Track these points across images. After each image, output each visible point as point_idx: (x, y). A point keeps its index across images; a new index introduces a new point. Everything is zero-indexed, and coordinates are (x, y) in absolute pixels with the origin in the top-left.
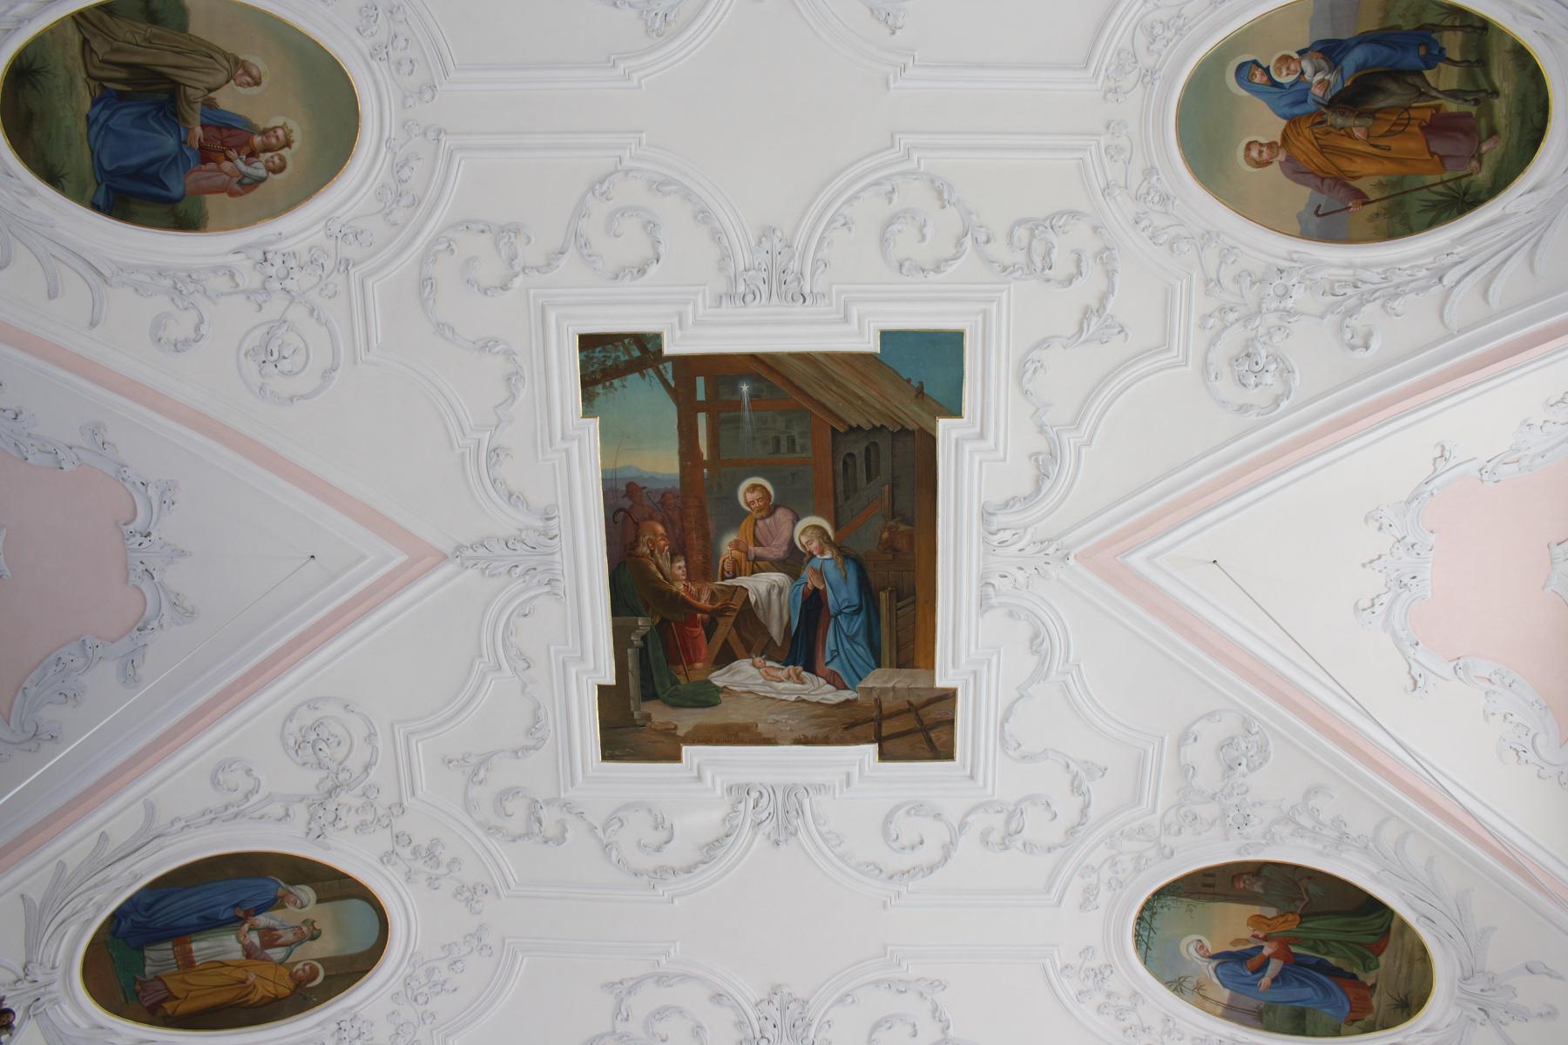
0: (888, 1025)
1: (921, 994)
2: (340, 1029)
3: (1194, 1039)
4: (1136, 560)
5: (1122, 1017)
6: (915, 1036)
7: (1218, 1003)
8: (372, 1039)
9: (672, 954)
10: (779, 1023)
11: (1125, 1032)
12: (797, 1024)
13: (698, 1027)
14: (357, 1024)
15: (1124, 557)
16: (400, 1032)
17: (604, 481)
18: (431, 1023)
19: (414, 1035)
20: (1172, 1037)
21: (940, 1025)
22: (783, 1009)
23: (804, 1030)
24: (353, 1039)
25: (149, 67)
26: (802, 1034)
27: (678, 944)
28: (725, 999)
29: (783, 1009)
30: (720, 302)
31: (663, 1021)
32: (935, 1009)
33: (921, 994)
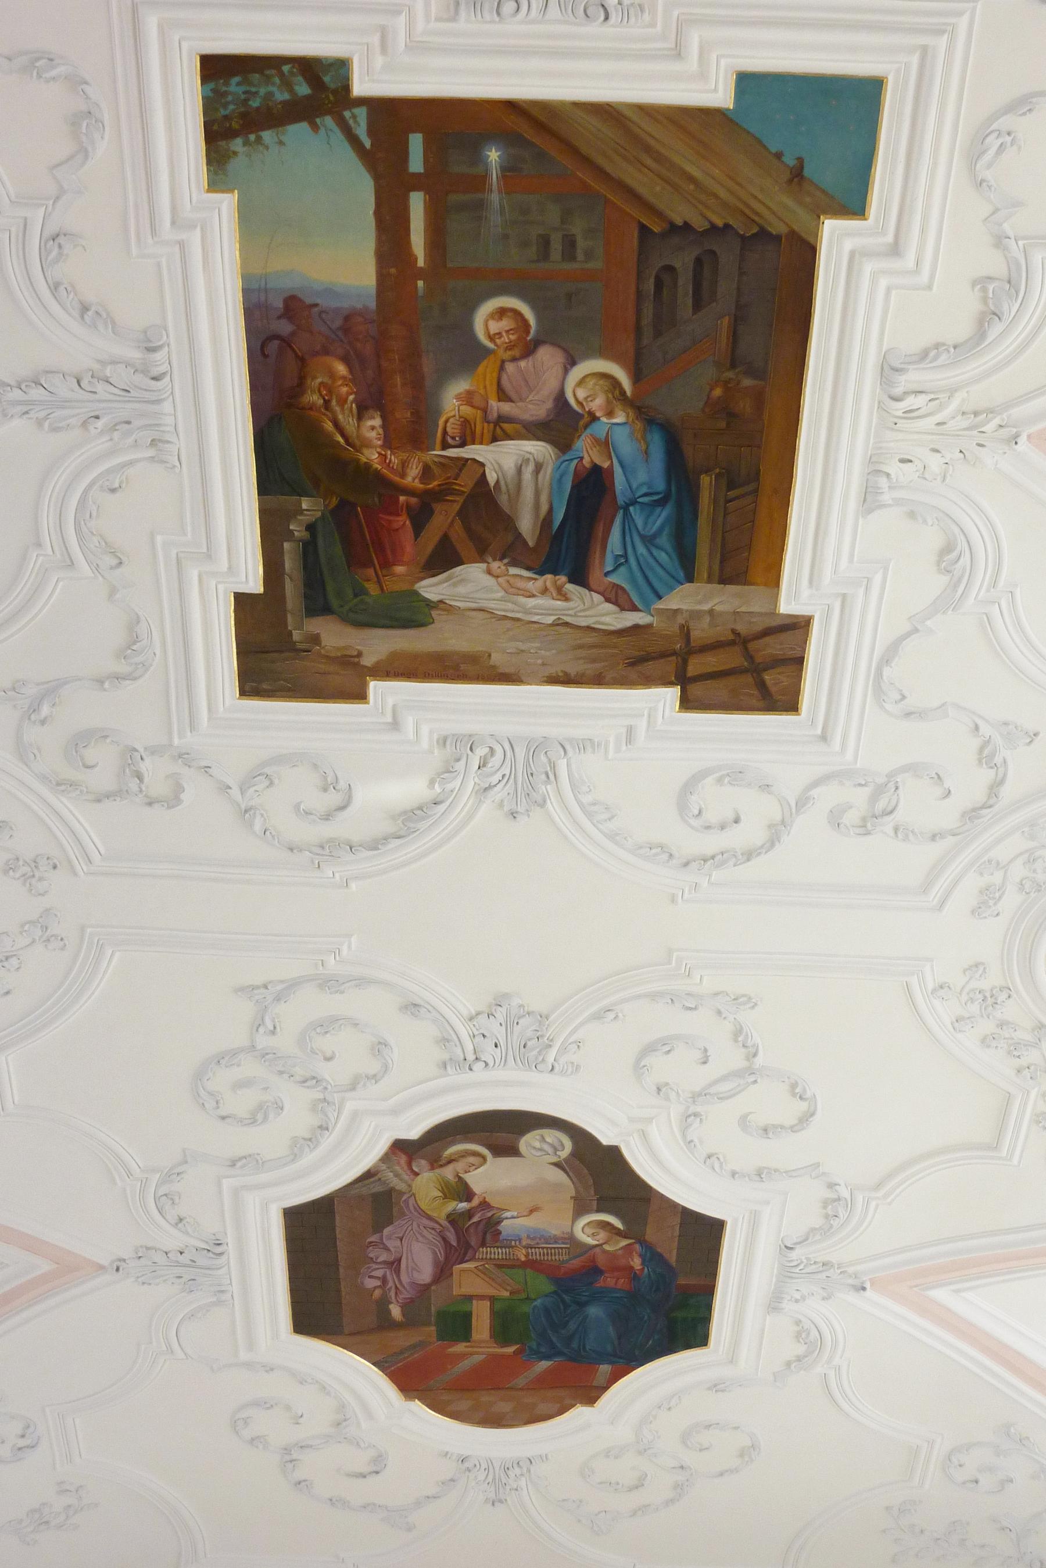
27: (354, 939)
29: (510, 1024)
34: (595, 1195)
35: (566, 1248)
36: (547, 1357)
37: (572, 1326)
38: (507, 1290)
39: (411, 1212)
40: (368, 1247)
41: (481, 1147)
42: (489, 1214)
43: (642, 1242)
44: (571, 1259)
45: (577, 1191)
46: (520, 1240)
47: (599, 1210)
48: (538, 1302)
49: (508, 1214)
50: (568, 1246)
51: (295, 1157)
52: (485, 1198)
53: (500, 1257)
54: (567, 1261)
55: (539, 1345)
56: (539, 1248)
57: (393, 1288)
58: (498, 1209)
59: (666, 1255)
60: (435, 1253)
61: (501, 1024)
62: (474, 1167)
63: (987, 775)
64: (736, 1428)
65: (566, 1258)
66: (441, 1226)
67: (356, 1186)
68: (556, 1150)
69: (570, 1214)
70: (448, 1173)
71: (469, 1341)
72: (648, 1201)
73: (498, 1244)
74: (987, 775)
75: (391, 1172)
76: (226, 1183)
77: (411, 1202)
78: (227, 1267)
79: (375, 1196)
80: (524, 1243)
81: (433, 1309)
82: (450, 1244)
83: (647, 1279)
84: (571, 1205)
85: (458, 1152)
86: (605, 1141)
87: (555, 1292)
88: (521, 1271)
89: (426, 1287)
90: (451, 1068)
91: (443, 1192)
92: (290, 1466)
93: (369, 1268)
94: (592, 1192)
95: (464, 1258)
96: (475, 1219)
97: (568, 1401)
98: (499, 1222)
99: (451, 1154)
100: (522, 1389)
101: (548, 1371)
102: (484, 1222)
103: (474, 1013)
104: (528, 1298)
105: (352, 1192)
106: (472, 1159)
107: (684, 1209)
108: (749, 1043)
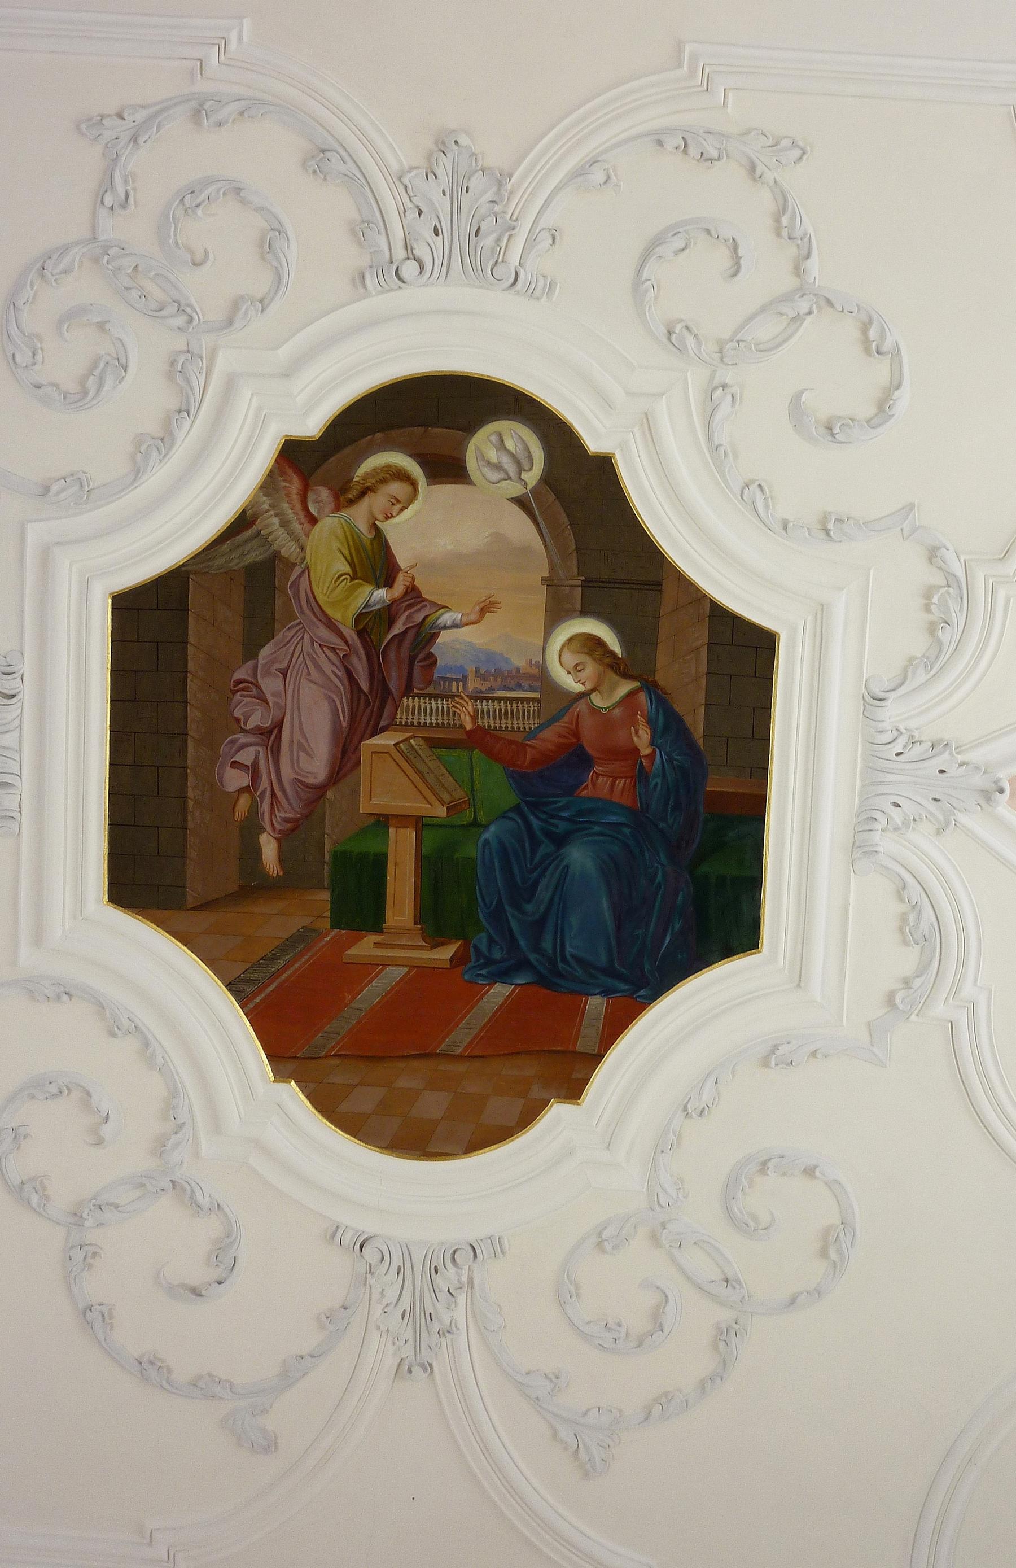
0: (679, 243)
1: (752, 168)
6: (734, 275)
9: (233, 45)
17: (315, 525)
22: (457, 191)
25: (334, 622)
27: (247, 23)
28: (334, 157)
29: (457, 191)
32: (783, 207)
33: (752, 168)
34: (579, 575)
35: (533, 700)
36: (502, 975)
37: (544, 893)
38: (442, 802)
39: (302, 611)
40: (234, 693)
41: (409, 459)
42: (419, 617)
43: (650, 686)
44: (542, 727)
45: (552, 568)
46: (465, 679)
47: (585, 612)
48: (490, 834)
49: (447, 618)
50: (537, 695)
51: (137, 473)
52: (413, 579)
53: (434, 721)
54: (532, 734)
55: (491, 941)
56: (493, 699)
57: (268, 793)
58: (434, 604)
59: (688, 720)
60: (335, 711)
61: (444, 194)
62: (398, 506)
63: (908, 960)
64: (810, 1172)
65: (533, 723)
66: (346, 643)
67: (224, 547)
68: (520, 469)
69: (540, 618)
70: (359, 515)
71: (381, 932)
72: (657, 586)
73: (430, 690)
74: (908, 960)
75: (276, 515)
76: (35, 533)
77: (304, 583)
78: (16, 734)
79: (251, 570)
80: (471, 687)
81: (327, 846)
82: (359, 687)
83: (659, 780)
84: (540, 597)
85: (375, 472)
86: (594, 445)
87: (517, 809)
88: (464, 754)
89: (321, 789)
90: (372, 275)
91: (351, 564)
92: (78, 1255)
93: (233, 742)
94: (575, 571)
95: (377, 723)
96: (398, 628)
97: (537, 1092)
98: (434, 636)
99: (366, 477)
100: (461, 1057)
101: (509, 1009)
102: (411, 634)
103: (406, 166)
104: (475, 824)
105: (217, 562)
106: (396, 488)
107: (715, 606)
108: (798, 233)
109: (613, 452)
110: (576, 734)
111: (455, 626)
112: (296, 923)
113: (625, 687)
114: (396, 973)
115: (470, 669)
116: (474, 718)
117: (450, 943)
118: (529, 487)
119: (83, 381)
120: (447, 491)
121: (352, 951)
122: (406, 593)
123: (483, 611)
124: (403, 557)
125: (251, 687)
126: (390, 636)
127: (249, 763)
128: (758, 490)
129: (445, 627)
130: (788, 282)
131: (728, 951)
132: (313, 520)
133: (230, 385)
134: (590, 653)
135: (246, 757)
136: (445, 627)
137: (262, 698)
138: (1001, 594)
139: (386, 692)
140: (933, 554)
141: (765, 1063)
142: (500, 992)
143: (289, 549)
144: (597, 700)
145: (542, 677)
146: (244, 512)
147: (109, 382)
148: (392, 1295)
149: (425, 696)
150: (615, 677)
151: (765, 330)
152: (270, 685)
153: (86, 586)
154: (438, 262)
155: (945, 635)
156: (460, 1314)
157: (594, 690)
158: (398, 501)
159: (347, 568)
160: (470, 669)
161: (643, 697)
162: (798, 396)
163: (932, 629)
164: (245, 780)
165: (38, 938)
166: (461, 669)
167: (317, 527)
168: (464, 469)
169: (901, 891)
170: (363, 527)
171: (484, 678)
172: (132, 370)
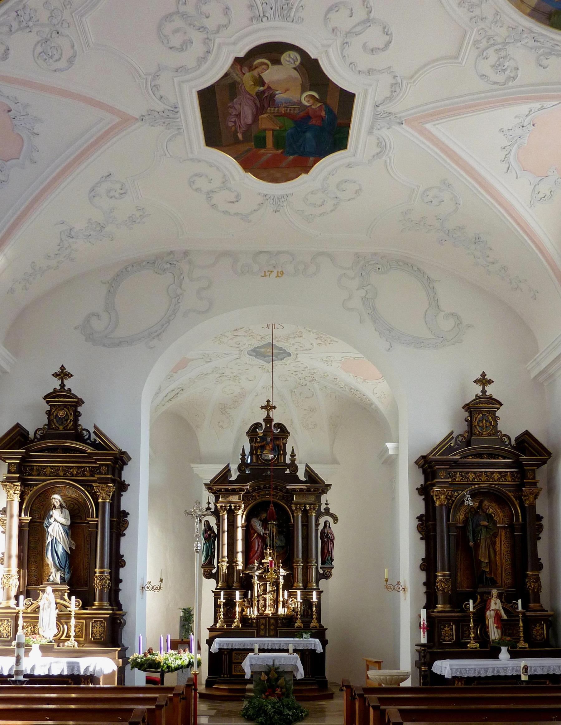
0: (337, 9)
2: (18, 15)
3: (509, 27)
4: (429, 126)
5: (471, 10)
6: (351, 16)
7: (529, 6)
8: (38, 21)
10: (274, 7)
11: (471, 19)
12: (284, 7)
13: (226, 8)
14: (27, 12)
15: (423, 124)
16: (53, 15)
18: (70, 8)
19: (62, 17)
20: (496, 25)
21: (367, 10)
23: (288, 11)
24: (28, 22)
26: (287, 14)
30: (252, 20)
31: (206, 5)
43: (325, 104)
45: (302, 82)
46: (282, 104)
47: (310, 90)
49: (277, 92)
51: (199, 66)
56: (289, 107)
58: (274, 90)
62: (265, 70)
68: (294, 62)
70: (255, 73)
74: (378, 150)
76: (175, 79)
77: (243, 87)
80: (284, 105)
81: (253, 135)
83: (326, 121)
84: (300, 88)
86: (313, 57)
91: (254, 82)
96: (266, 95)
99: (256, 64)
102: (269, 96)
106: (264, 67)
107: (341, 88)
108: (369, 6)
109: (317, 58)
110: (308, 113)
111: (279, 94)
112: (247, 148)
113: (319, 104)
114: (269, 155)
115: (284, 102)
116: (284, 111)
117: (280, 150)
118: (297, 65)
119: (182, 46)
120: (276, 67)
121: (259, 152)
122: (267, 88)
123: (286, 91)
124: (266, 81)
125: (233, 107)
126: (264, 96)
127: (234, 121)
128: (353, 65)
129: (277, 94)
130: (365, 17)
131: (340, 149)
132: (244, 74)
133: (219, 47)
134: (311, 98)
135: (233, 120)
136: (277, 94)
137: (235, 109)
138: (409, 85)
139: (264, 106)
140: (395, 77)
141: (347, 167)
142: (291, 157)
143: (239, 80)
144: (313, 107)
145: (300, 103)
146: (227, 72)
147: (189, 46)
148: (271, 202)
149: (273, 107)
150: (317, 103)
151: (358, 29)
152: (237, 106)
153: (191, 91)
154: (272, 17)
155: (395, 94)
156: (285, 204)
157: (312, 105)
158: (264, 69)
159: (253, 83)
160: (284, 102)
161: (323, 106)
162: (366, 43)
163: (392, 92)
164: (233, 124)
165: (192, 153)
166: (281, 102)
167: (245, 76)
168: (281, 63)
169: (378, 139)
170: (256, 75)
171: (286, 103)
172: (194, 43)
